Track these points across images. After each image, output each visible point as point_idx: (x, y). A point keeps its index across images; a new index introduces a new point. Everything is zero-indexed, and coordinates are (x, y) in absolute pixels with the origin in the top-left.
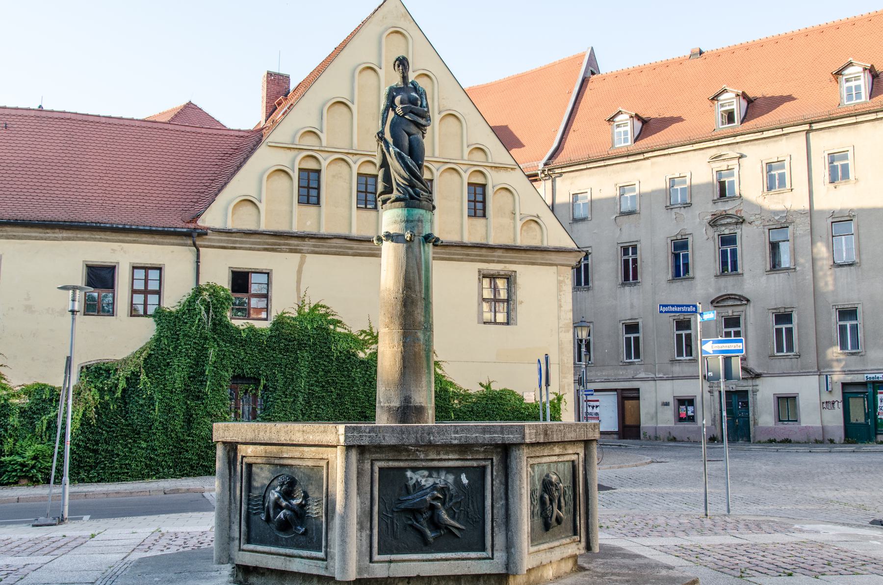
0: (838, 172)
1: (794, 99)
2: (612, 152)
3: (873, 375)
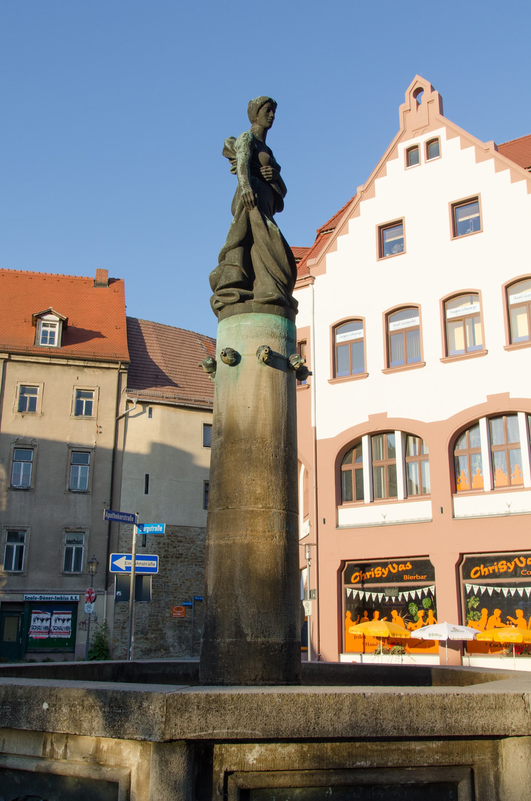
0: (27, 404)
1: (103, 337)
2: (33, 349)
3: (32, 596)
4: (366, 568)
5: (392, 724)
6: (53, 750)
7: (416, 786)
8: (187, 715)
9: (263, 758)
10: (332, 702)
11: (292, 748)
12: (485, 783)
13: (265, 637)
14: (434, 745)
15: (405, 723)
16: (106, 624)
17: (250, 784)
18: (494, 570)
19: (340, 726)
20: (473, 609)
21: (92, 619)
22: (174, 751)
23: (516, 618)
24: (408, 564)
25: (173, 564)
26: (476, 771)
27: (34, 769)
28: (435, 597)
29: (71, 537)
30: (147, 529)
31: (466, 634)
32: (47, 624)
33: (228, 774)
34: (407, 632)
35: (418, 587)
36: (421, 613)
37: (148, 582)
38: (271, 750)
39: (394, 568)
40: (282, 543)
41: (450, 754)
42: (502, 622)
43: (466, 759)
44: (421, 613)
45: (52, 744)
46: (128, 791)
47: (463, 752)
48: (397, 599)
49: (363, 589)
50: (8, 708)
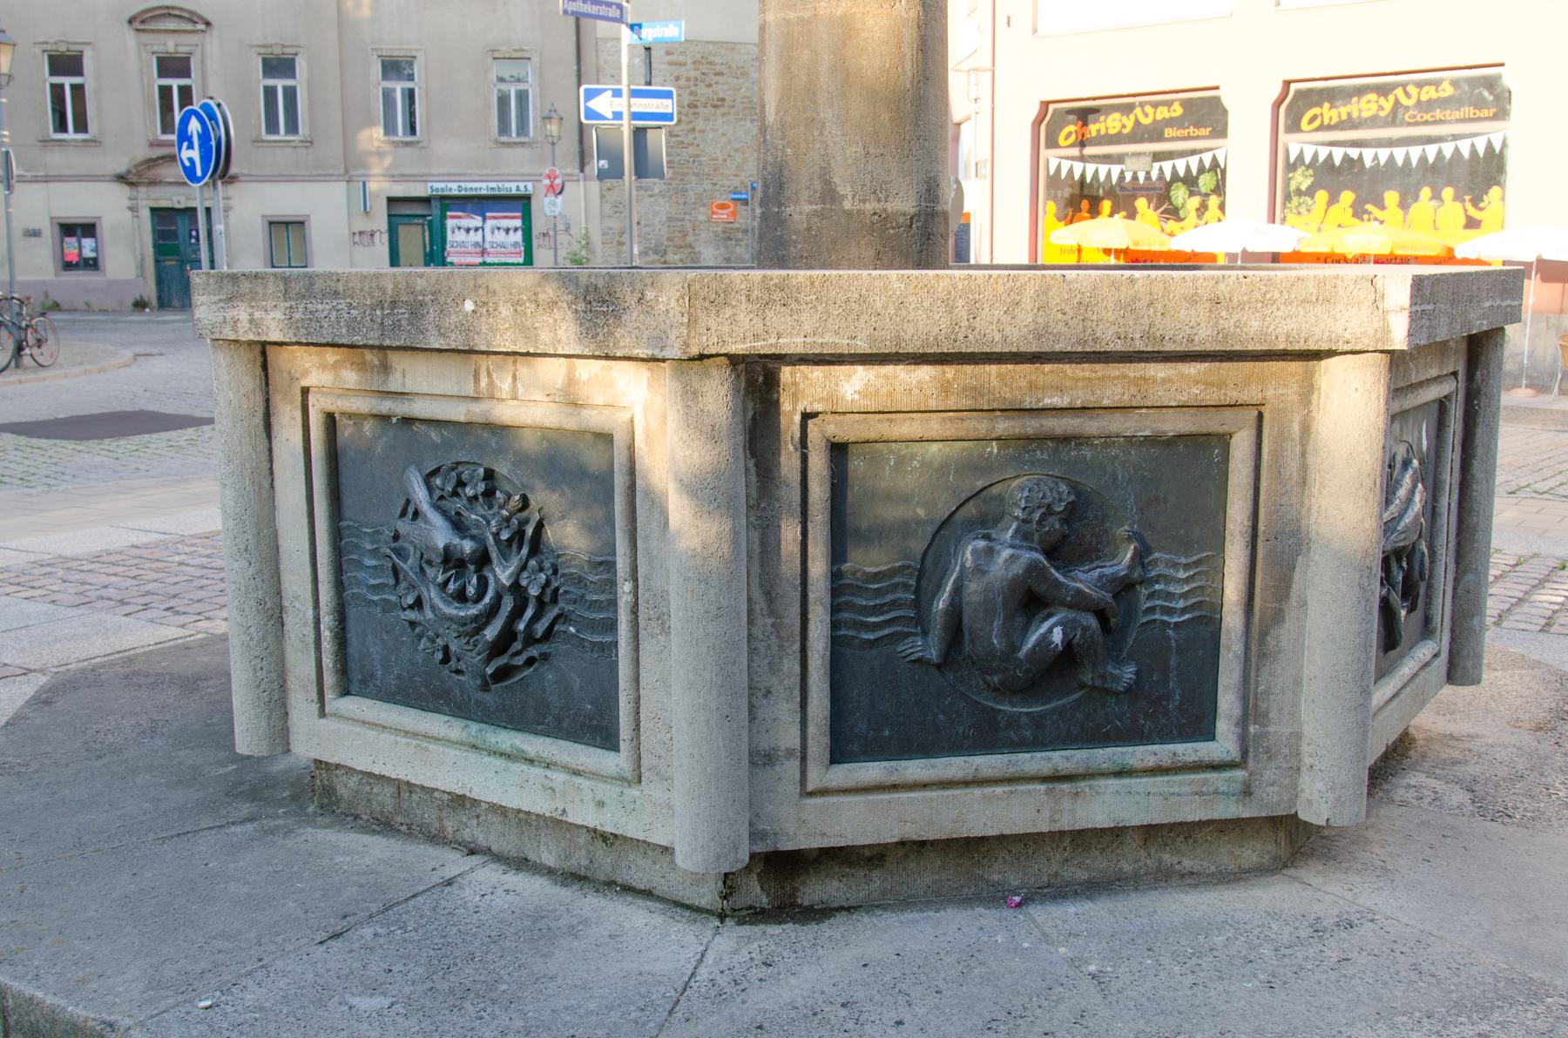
3: (442, 185)
4: (1091, 117)
5: (1114, 329)
6: (491, 384)
7: (1153, 441)
8: (728, 312)
9: (871, 389)
10: (1001, 289)
11: (925, 372)
12: (1283, 435)
13: (879, 200)
14: (1192, 370)
15: (1139, 329)
16: (587, 236)
17: (845, 431)
18: (1349, 114)
19: (1016, 333)
20: (1299, 193)
21: (561, 227)
22: (707, 375)
23: (1383, 208)
24: (1176, 106)
25: (707, 120)
26: (1266, 416)
27: (462, 418)
28: (1224, 172)
29: (507, 70)
30: (650, 34)
31: (1282, 239)
32: (478, 237)
33: (807, 416)
34: (1165, 238)
35: (1193, 152)
36: (1195, 202)
37: (659, 141)
38: (886, 377)
39: (1146, 115)
40: (913, 14)
41: (1222, 385)
42: (1354, 215)
43: (1251, 394)
44: (1195, 202)
45: (489, 375)
46: (631, 447)
47: (1247, 382)
48: (1148, 177)
49: (1082, 159)
50: (402, 313)
